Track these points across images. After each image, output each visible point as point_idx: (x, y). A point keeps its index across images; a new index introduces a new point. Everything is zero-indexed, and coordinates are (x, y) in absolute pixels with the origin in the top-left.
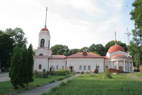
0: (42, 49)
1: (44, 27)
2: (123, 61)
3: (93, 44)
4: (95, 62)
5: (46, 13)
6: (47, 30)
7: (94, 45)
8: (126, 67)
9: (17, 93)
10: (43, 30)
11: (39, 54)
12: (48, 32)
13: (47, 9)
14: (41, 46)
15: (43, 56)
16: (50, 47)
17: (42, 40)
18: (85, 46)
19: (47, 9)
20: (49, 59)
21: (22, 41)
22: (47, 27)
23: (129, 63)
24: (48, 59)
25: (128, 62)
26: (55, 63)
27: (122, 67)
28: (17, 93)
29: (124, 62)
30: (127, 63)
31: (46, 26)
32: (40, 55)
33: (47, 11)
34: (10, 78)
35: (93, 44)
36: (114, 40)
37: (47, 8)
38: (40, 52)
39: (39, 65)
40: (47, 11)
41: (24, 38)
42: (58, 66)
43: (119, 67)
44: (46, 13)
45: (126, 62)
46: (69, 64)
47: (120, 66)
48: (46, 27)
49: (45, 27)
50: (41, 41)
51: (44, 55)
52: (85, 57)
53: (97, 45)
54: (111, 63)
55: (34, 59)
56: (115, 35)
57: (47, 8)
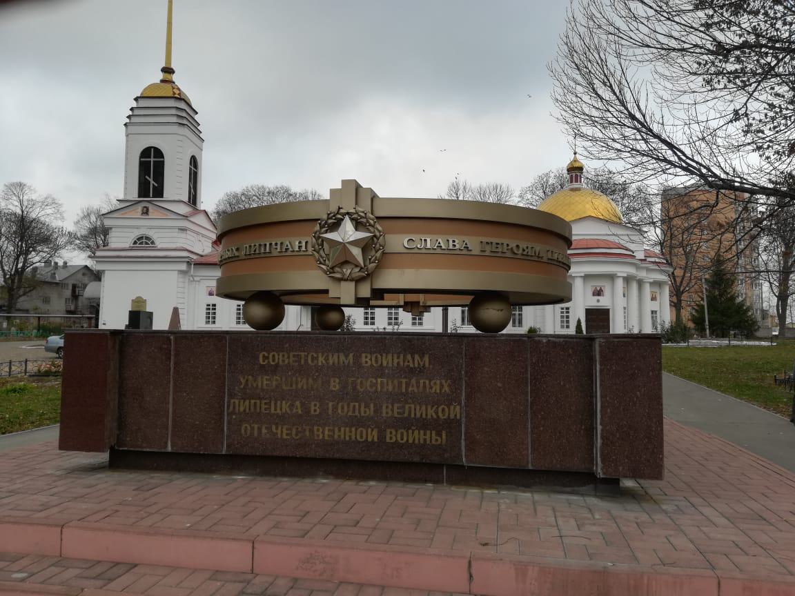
14: (144, 190)
17: (146, 153)
29: (620, 283)
30: (634, 286)
31: (168, 70)
38: (138, 227)
45: (628, 280)
50: (141, 164)
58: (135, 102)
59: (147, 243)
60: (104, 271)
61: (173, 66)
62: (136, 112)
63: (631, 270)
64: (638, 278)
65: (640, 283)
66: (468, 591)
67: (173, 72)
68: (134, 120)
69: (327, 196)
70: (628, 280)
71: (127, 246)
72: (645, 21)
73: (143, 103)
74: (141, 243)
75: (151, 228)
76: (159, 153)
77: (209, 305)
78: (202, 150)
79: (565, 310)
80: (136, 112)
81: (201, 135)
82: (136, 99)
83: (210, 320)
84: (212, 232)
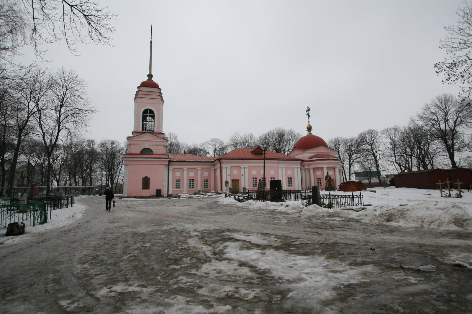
0: (147, 137)
1: (146, 78)
4: (284, 170)
5: (151, 42)
6: (155, 86)
9: (341, 245)
10: (144, 85)
11: (140, 150)
15: (153, 154)
17: (146, 111)
20: (171, 163)
22: (154, 79)
24: (167, 163)
25: (309, 170)
26: (185, 172)
27: (279, 182)
28: (339, 244)
30: (307, 171)
31: (150, 76)
32: (142, 151)
39: (143, 178)
41: (421, 123)
42: (291, 178)
43: (232, 180)
44: (151, 42)
46: (229, 173)
48: (153, 79)
51: (155, 152)
52: (258, 157)
55: (451, 165)
71: (139, 153)
76: (152, 112)
77: (205, 180)
79: (192, 181)
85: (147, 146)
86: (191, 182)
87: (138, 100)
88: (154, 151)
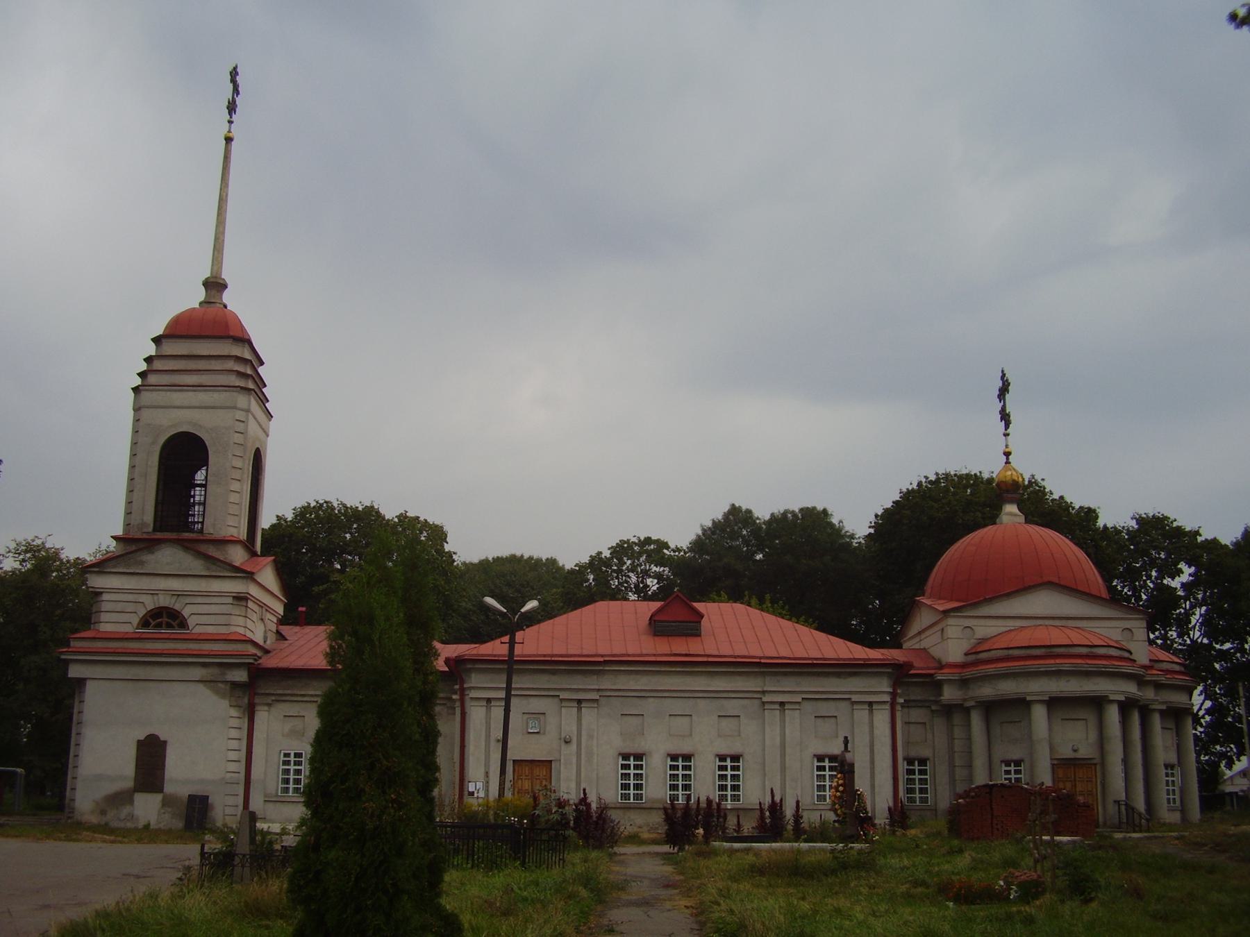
2: (1097, 703)
3: (734, 510)
5: (229, 140)
7: (737, 518)
8: (1126, 761)
12: (237, 350)
13: (236, 90)
14: (162, 521)
16: (266, 520)
18: (633, 531)
19: (236, 90)
21: (33, 562)
23: (1156, 721)
29: (1113, 714)
30: (1136, 718)
31: (215, 285)
32: (145, 623)
33: (232, 108)
34: (822, 509)
35: (734, 510)
36: (988, 466)
37: (234, 74)
38: (154, 593)
39: (141, 744)
40: (232, 108)
44: (229, 140)
45: (1126, 707)
47: (1066, 752)
49: (201, 294)
53: (781, 523)
54: (968, 725)
56: (1005, 417)
57: (234, 81)
58: (153, 345)
59: (169, 626)
60: (85, 679)
61: (1004, 437)
62: (158, 365)
63: (1131, 688)
64: (1141, 703)
65: (1145, 712)
66: (875, 707)
67: (225, 286)
68: (152, 379)
69: (447, 548)
70: (1126, 707)
72: (516, 790)
73: (170, 348)
74: (159, 626)
75: (178, 595)
77: (287, 755)
78: (268, 436)
80: (158, 365)
81: (267, 405)
82: (157, 340)
83: (291, 786)
84: (244, 577)
85: (164, 601)
86: (733, 768)
87: (147, 397)
88: (191, 622)
